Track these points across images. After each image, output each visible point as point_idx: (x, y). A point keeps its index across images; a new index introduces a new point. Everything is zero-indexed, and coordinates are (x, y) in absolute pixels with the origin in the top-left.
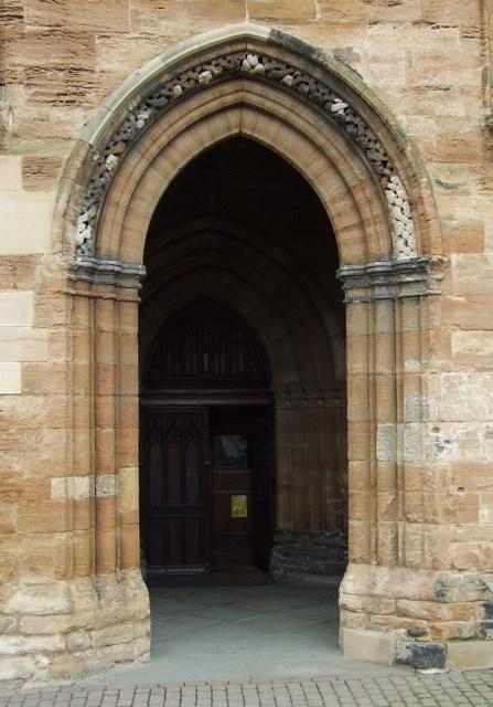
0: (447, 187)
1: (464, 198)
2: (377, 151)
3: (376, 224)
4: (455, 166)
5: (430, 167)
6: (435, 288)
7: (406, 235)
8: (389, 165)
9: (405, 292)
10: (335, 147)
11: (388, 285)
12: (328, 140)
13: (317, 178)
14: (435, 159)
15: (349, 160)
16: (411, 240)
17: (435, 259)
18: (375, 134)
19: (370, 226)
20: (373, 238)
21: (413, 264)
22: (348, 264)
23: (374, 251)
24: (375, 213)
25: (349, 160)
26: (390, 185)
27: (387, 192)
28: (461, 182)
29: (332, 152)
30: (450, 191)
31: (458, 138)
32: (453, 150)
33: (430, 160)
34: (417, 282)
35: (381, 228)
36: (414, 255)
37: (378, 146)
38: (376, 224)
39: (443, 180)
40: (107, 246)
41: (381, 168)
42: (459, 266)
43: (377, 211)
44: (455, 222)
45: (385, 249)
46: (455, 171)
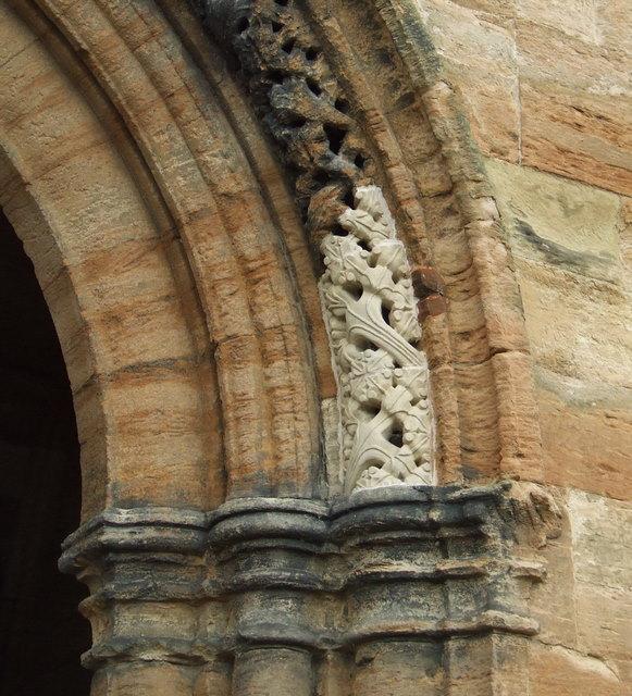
0: (554, 255)
1: (601, 308)
2: (314, 87)
3: (266, 359)
4: (577, 194)
5: (497, 173)
6: (513, 607)
7: (396, 399)
8: (353, 141)
9: (377, 617)
10: (144, 63)
11: (303, 592)
12: (120, 30)
13: (45, 170)
14: (515, 154)
15: (189, 112)
16: (418, 424)
17: (521, 492)
18: (314, 26)
19: (236, 362)
20: (253, 409)
21: (429, 504)
22: (130, 504)
23: (251, 456)
24: (268, 318)
25: (189, 112)
26: (348, 216)
27: (329, 242)
28: (595, 250)
29: (128, 78)
30: (561, 271)
31: (586, 103)
32: (567, 138)
33: (501, 153)
34: (438, 580)
35: (289, 374)
36: (424, 477)
37: (318, 69)
38: (266, 359)
39: (541, 230)
40: (139, 680)
41: (323, 148)
42: (593, 540)
43: (278, 310)
44: (572, 383)
45: (297, 455)
46: (578, 209)
